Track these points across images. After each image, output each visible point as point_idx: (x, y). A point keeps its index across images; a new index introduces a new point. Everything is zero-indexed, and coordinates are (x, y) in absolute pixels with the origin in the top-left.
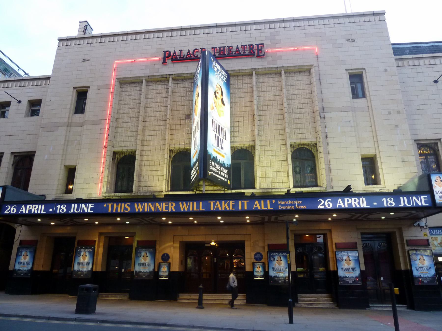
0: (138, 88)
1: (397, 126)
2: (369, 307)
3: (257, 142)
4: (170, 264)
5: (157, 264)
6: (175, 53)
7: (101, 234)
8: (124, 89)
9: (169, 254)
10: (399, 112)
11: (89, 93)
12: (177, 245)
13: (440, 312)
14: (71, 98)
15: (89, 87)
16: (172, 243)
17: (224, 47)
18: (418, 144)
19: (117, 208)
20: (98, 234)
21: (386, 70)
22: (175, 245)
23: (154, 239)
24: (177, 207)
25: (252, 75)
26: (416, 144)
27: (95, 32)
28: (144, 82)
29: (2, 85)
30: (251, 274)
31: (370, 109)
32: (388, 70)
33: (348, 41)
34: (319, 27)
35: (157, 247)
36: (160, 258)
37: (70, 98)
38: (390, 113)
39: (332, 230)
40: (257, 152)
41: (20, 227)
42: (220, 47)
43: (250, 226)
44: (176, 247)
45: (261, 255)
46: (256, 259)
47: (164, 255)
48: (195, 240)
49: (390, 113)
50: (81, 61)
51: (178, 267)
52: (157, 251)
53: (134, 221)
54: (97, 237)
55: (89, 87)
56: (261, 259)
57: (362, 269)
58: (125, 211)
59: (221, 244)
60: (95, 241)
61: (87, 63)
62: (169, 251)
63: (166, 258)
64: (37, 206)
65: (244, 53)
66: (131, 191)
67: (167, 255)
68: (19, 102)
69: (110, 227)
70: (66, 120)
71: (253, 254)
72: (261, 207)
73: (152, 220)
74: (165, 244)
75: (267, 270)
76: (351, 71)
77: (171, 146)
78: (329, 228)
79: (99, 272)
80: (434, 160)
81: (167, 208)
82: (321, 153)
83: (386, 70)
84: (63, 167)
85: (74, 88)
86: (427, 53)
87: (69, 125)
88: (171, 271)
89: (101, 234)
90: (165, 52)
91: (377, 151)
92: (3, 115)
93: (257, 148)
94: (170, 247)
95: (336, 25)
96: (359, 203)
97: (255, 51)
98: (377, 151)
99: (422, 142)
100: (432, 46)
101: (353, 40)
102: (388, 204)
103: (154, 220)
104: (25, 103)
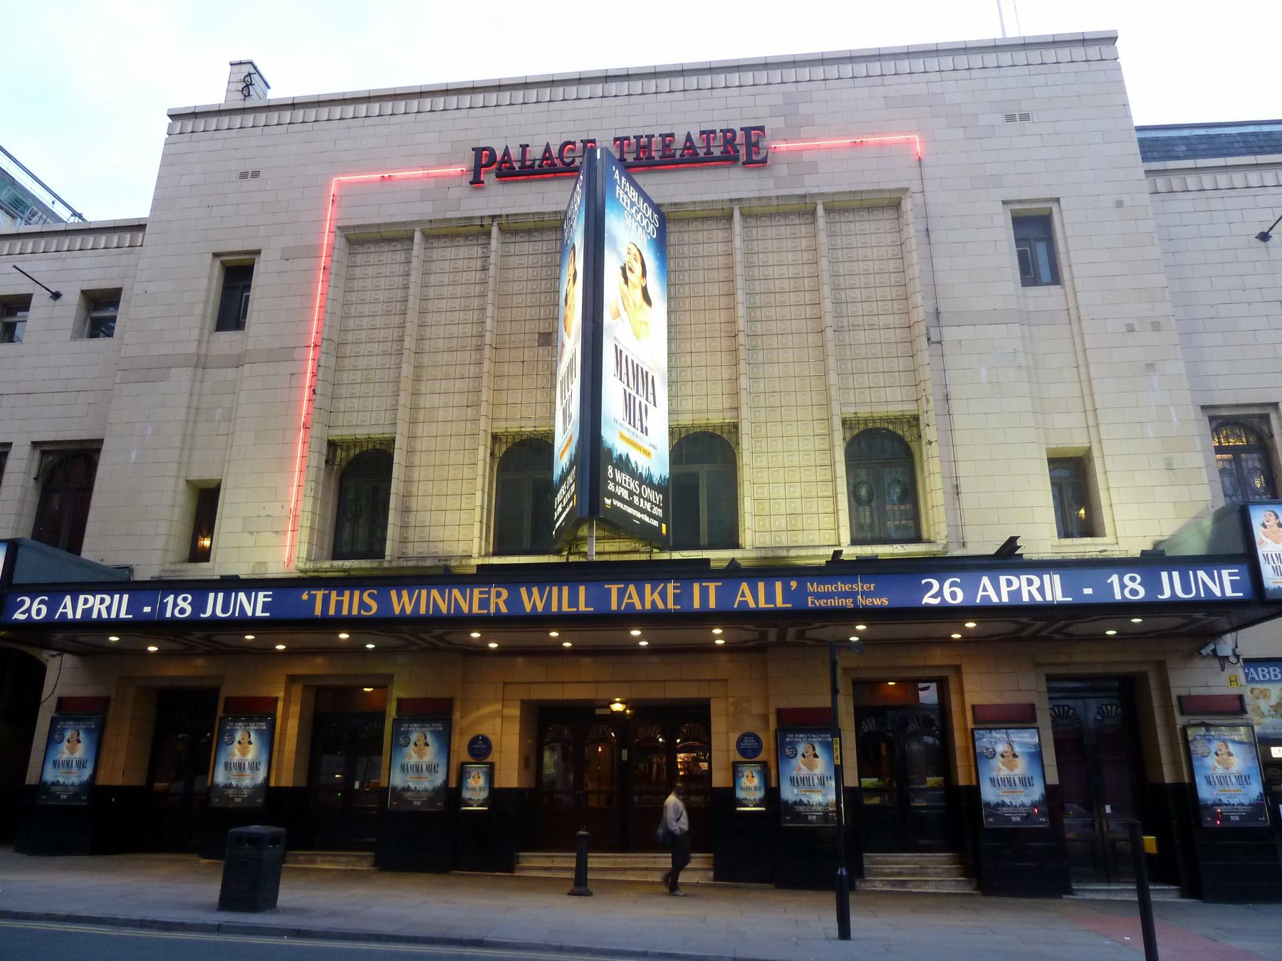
0: (400, 256)
1: (1151, 366)
2: (1070, 891)
3: (745, 412)
4: (492, 765)
5: (454, 765)
6: (506, 152)
7: (292, 680)
8: (359, 259)
9: (490, 737)
10: (1156, 326)
11: (259, 269)
12: (515, 711)
13: (1275, 906)
14: (205, 285)
15: (258, 252)
16: (498, 706)
17: (650, 137)
18: (1211, 419)
19: (339, 604)
20: (283, 679)
21: (1119, 204)
22: (507, 712)
23: (446, 695)
24: (514, 601)
25: (730, 218)
26: (1207, 419)
27: (276, 93)
28: (418, 237)
29: (6, 246)
30: (729, 796)
31: (1072, 317)
32: (1126, 203)
33: (1010, 118)
34: (925, 77)
35: (456, 716)
36: (465, 748)
37: (204, 283)
38: (1131, 329)
39: (964, 669)
40: (746, 443)
41: (58, 658)
42: (638, 138)
43: (724, 657)
44: (512, 717)
45: (757, 739)
46: (743, 752)
47: (475, 740)
48: (566, 697)
49: (1131, 329)
50: (235, 176)
51: (515, 775)
52: (456, 730)
53: (388, 641)
54: (282, 687)
55: (258, 252)
56: (757, 751)
57: (1049, 782)
58: (363, 612)
59: (642, 710)
60: (276, 700)
61: (251, 183)
62: (489, 729)
63: (481, 748)
64: (108, 598)
65: (709, 153)
66: (381, 555)
67: (486, 741)
68: (56, 296)
69: (319, 660)
70: (192, 349)
71: (734, 738)
72: (757, 602)
73: (440, 638)
74: (478, 707)
75: (774, 784)
76: (1017, 207)
77: (496, 424)
78: (956, 662)
79: (286, 788)
80: (1257, 464)
81: (484, 603)
82: (930, 443)
83: (1119, 204)
84: (182, 484)
85: (216, 255)
86: (1239, 155)
87: (200, 363)
88: (497, 785)
89: (292, 680)
90: (478, 151)
91: (1094, 438)
92: (9, 334)
93: (745, 429)
94: (492, 716)
95: (975, 74)
96: (1041, 590)
97: (740, 149)
98: (1094, 438)
99: (1224, 413)
100: (1254, 134)
101: (1025, 117)
102: (1127, 592)
103: (448, 638)
104: (72, 299)
